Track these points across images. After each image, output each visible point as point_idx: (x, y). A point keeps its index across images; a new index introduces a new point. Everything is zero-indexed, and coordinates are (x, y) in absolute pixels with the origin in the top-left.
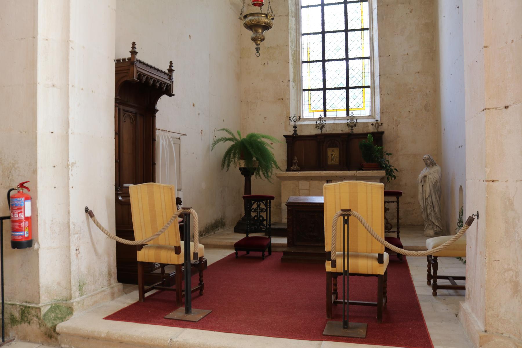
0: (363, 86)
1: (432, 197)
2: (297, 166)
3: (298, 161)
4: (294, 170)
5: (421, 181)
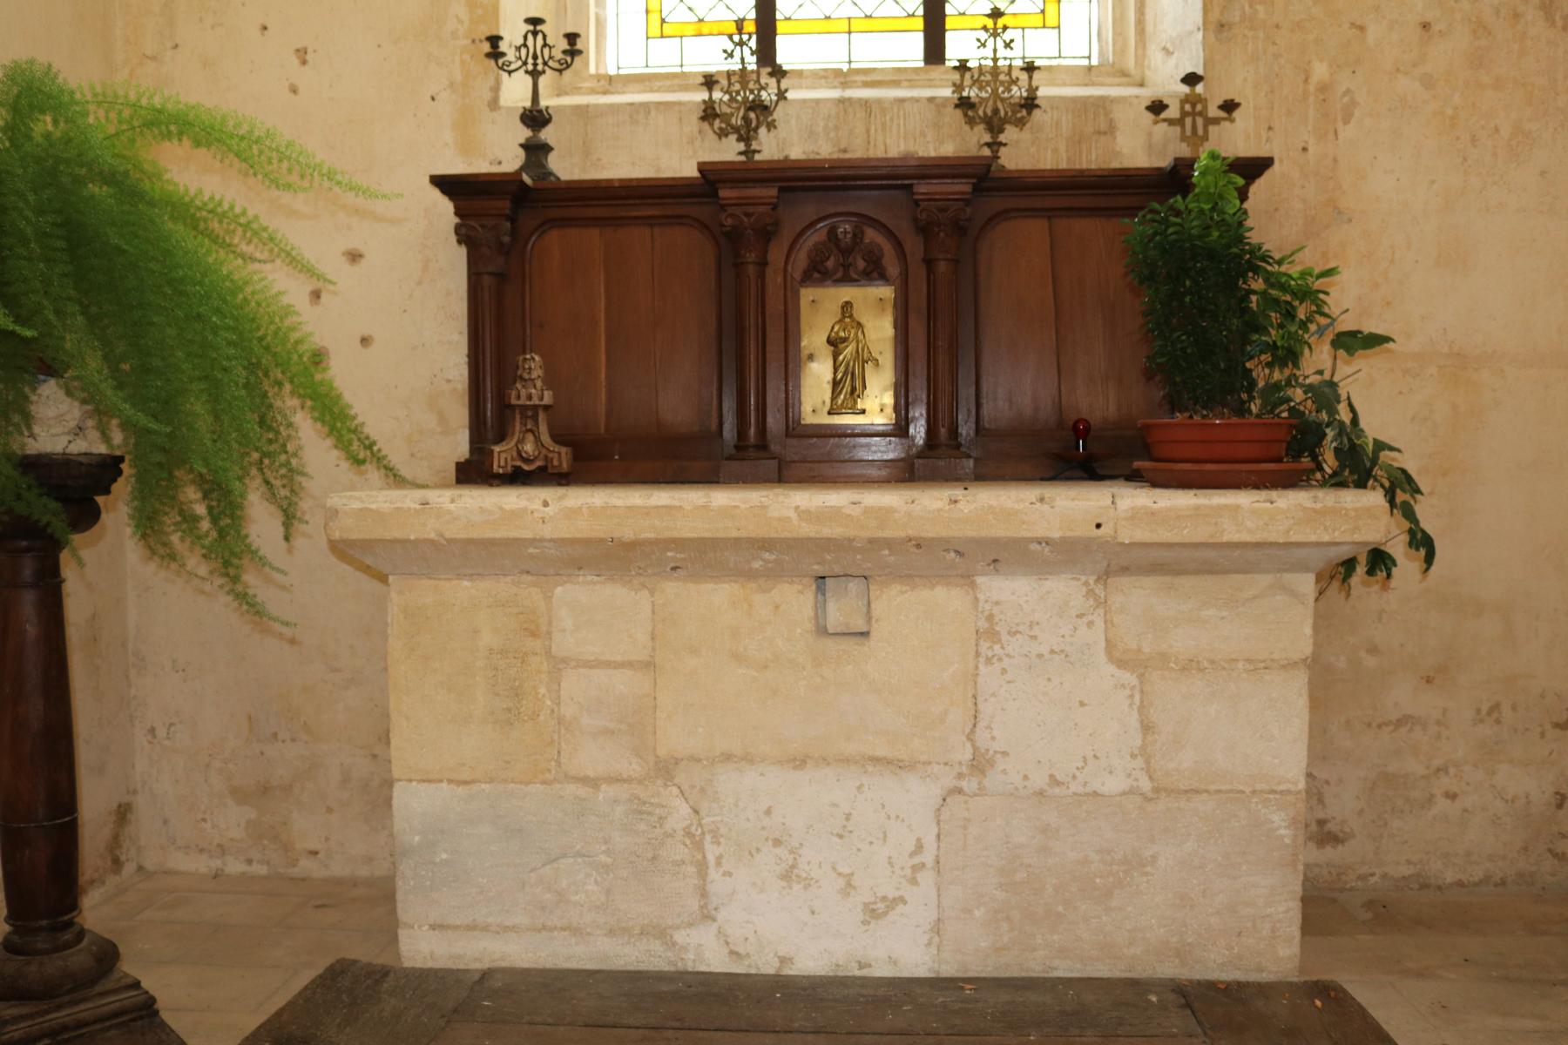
0: (943, 16)
2: (546, 438)
3: (555, 397)
4: (517, 470)
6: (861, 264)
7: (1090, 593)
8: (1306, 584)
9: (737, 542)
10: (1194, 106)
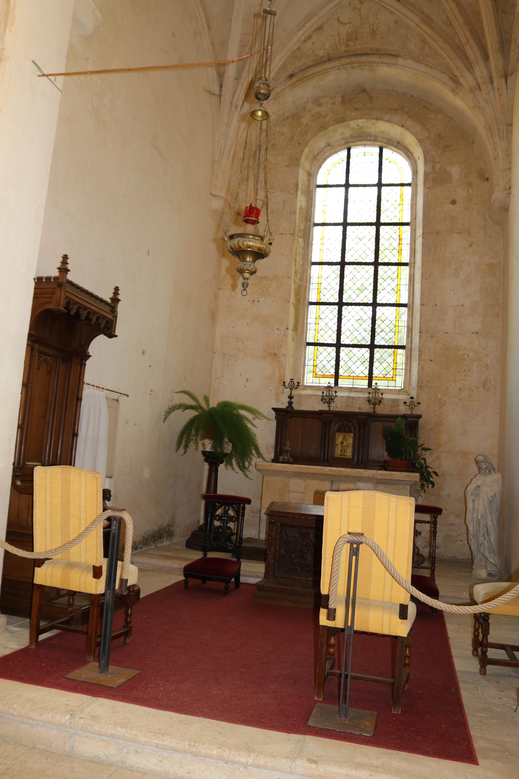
1: (487, 519)
5: (472, 494)
6: (347, 429)
7: (374, 486)
8: (408, 487)
9: (319, 474)
10: (412, 403)
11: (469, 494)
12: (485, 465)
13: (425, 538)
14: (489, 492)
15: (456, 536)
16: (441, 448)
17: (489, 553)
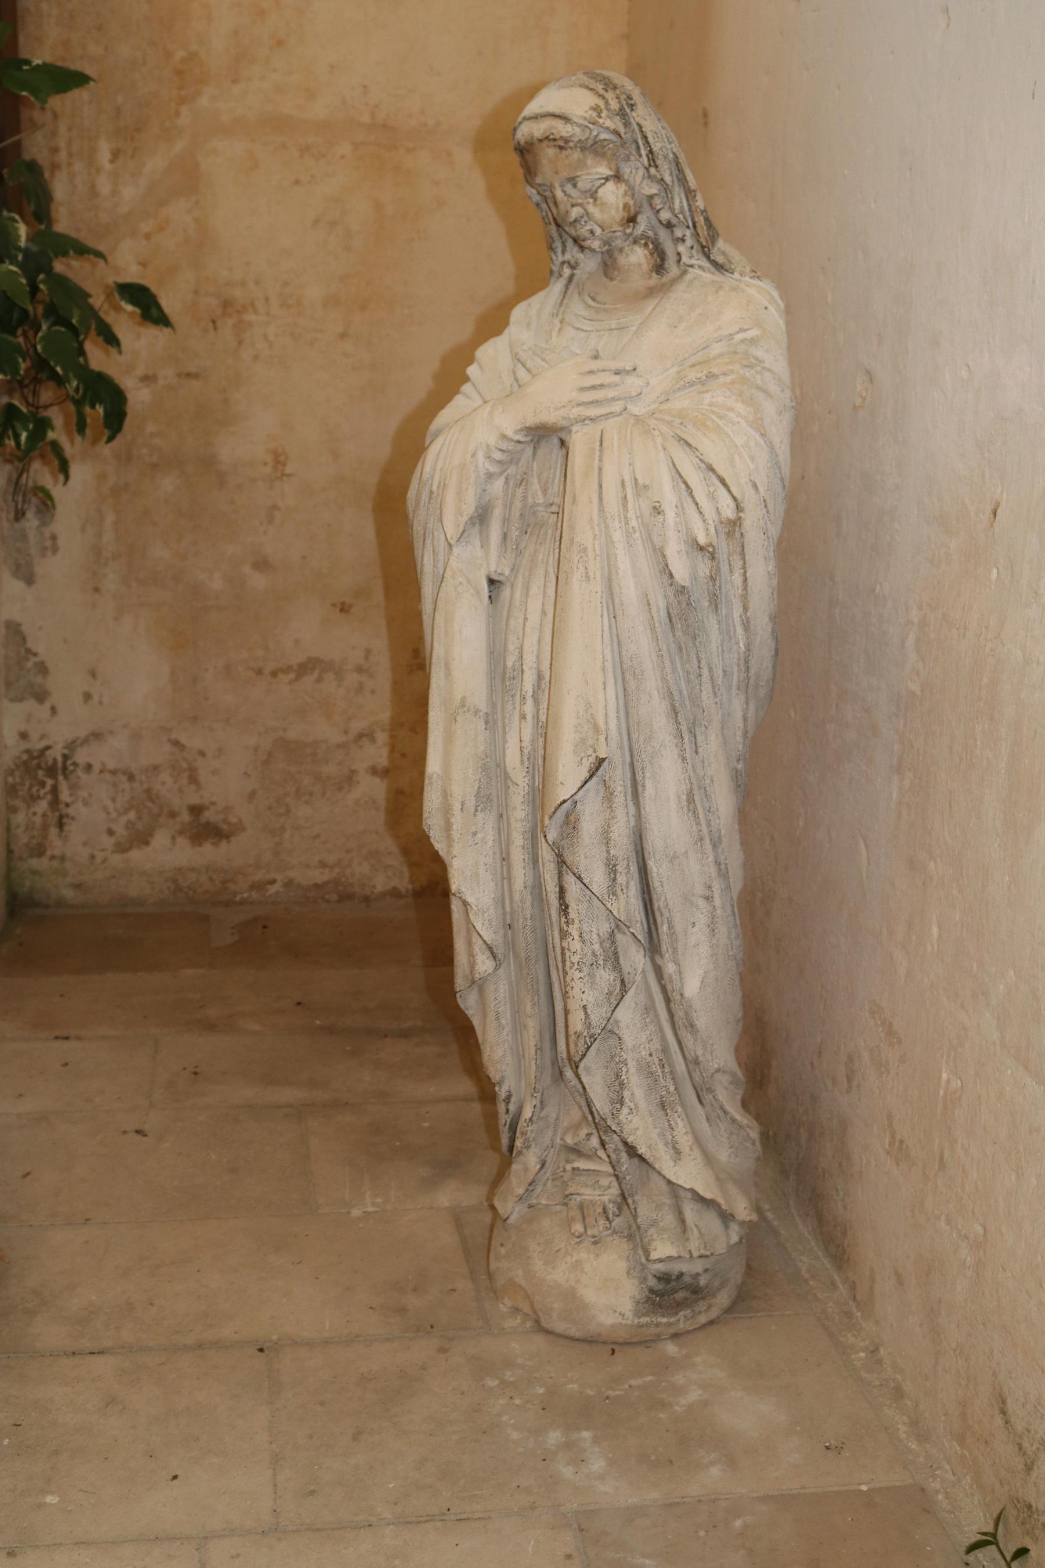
1: (648, 792)
5: (481, 517)
11: (451, 524)
12: (612, 194)
13: (131, 778)
14: (668, 495)
15: (339, 746)
16: (204, 101)
17: (663, 1106)
